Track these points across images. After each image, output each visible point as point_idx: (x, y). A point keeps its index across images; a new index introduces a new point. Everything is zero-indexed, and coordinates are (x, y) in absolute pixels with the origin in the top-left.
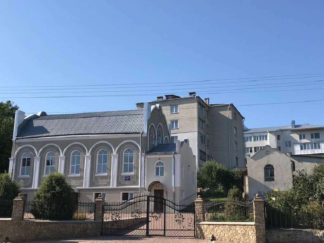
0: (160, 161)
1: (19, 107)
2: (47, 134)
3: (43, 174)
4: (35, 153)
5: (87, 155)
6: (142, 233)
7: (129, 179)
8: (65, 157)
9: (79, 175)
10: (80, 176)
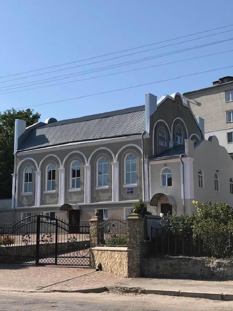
0: (166, 167)
1: (41, 114)
2: (46, 144)
3: (123, 184)
4: (35, 167)
5: (86, 165)
6: (62, 261)
7: (132, 192)
8: (64, 169)
9: (79, 189)
10: (80, 190)
